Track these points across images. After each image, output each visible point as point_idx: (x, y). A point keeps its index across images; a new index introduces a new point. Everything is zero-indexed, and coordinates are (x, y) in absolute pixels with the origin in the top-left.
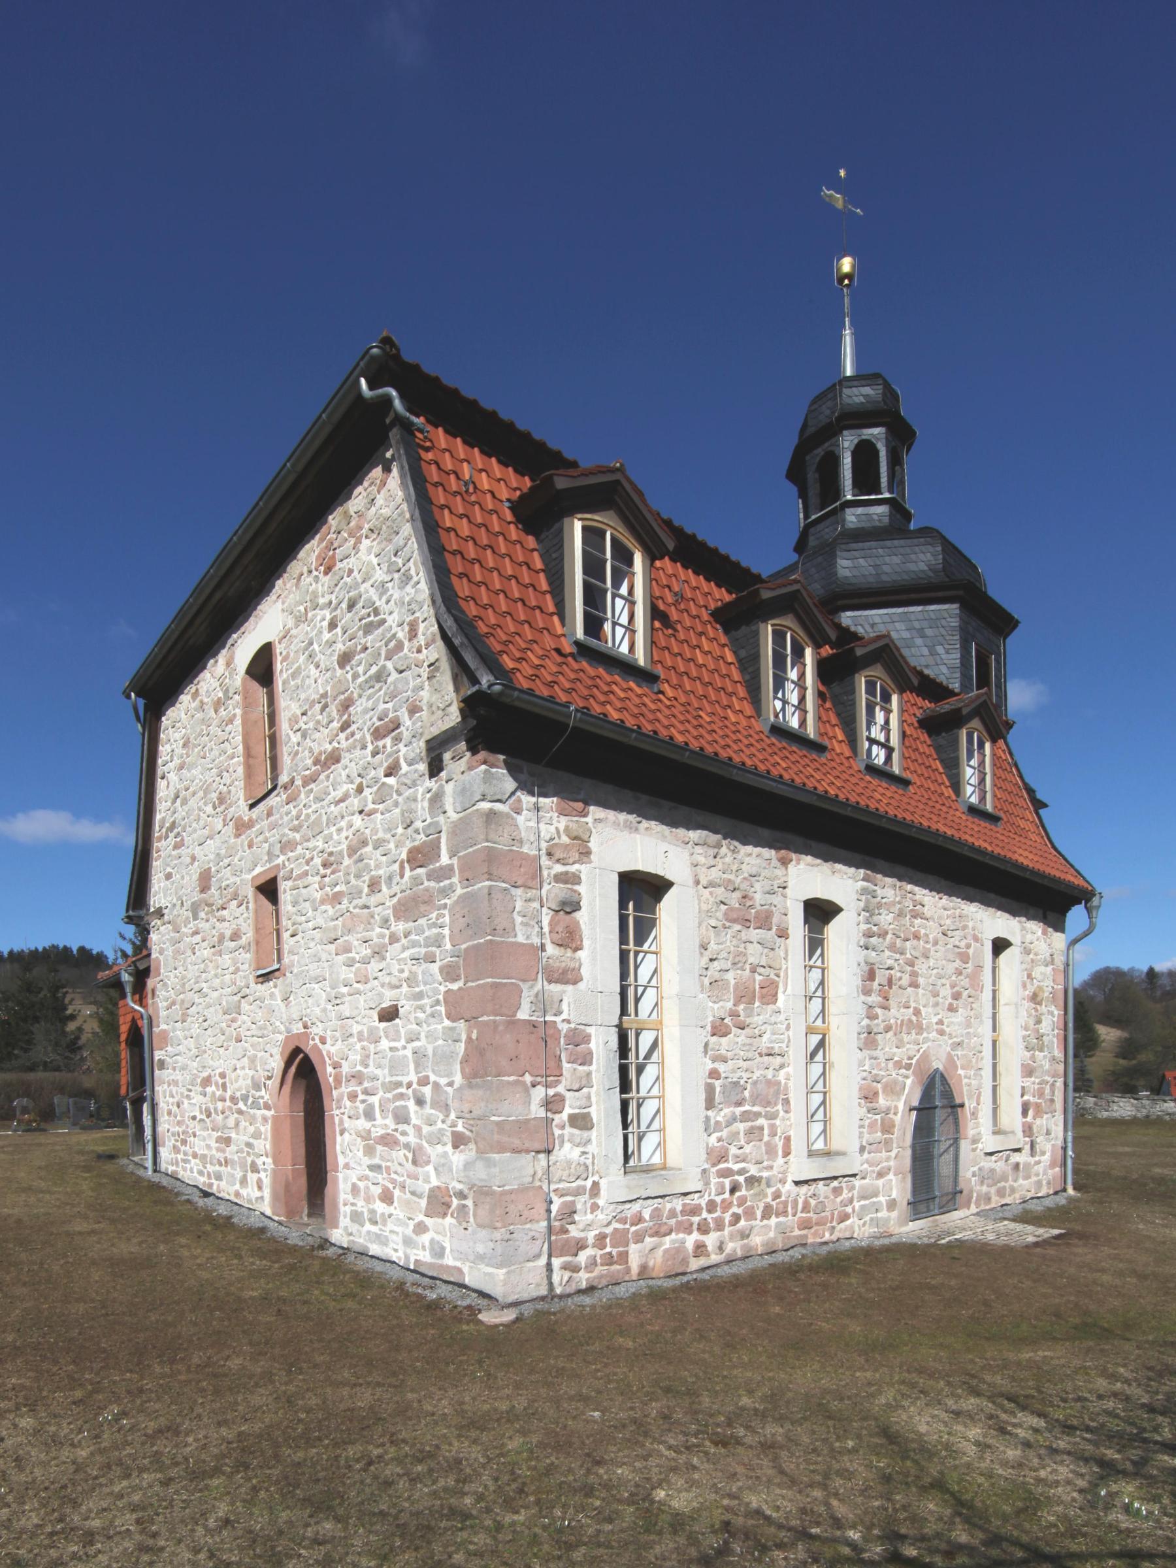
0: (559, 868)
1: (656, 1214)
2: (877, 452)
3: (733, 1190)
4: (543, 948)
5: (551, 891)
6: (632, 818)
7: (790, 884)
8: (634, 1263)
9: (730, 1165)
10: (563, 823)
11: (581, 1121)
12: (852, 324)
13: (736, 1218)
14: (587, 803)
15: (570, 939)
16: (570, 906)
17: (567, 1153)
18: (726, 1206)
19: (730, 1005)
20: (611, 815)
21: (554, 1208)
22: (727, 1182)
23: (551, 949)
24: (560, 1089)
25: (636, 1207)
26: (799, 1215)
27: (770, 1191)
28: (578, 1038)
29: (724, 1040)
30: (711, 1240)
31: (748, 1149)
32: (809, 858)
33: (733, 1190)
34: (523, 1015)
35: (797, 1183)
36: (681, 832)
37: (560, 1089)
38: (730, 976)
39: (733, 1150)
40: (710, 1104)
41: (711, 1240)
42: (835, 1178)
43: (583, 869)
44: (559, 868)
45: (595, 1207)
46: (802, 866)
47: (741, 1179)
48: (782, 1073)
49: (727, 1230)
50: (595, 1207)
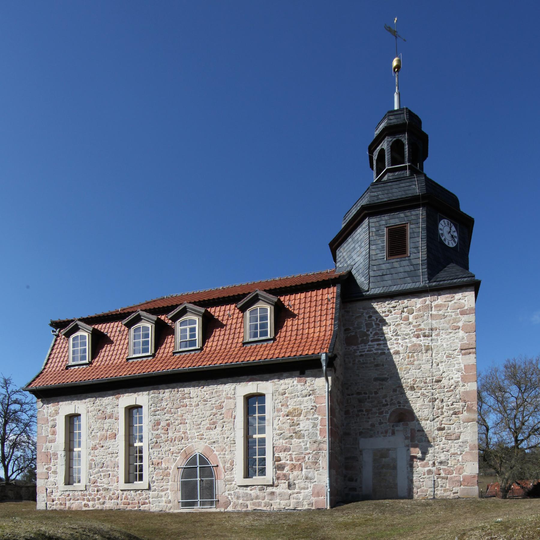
0: (52, 418)
1: (74, 495)
2: (403, 145)
3: (98, 491)
4: (48, 436)
5: (51, 424)
6: (70, 402)
7: (119, 404)
8: (67, 506)
9: (98, 484)
10: (53, 408)
11: (55, 472)
12: (399, 94)
13: (99, 499)
14: (58, 402)
15: (54, 433)
16: (54, 426)
17: (51, 479)
18: (96, 495)
19: (98, 441)
20: (64, 403)
21: (48, 491)
22: (96, 489)
23: (50, 436)
24: (51, 466)
25: (68, 493)
26: (123, 500)
27: (111, 492)
28: (55, 454)
29: (96, 451)
30: (90, 504)
31: (104, 480)
32: (127, 394)
33: (98, 491)
34: (43, 451)
35: (122, 490)
36: (84, 400)
37: (51, 466)
38: (99, 434)
39: (99, 480)
40: (90, 468)
41: (90, 504)
42: (253, 486)
43: (57, 417)
44: (52, 418)
45: (57, 492)
46: (125, 397)
47: (101, 488)
48: (117, 458)
49: (96, 502)
50: (57, 492)
